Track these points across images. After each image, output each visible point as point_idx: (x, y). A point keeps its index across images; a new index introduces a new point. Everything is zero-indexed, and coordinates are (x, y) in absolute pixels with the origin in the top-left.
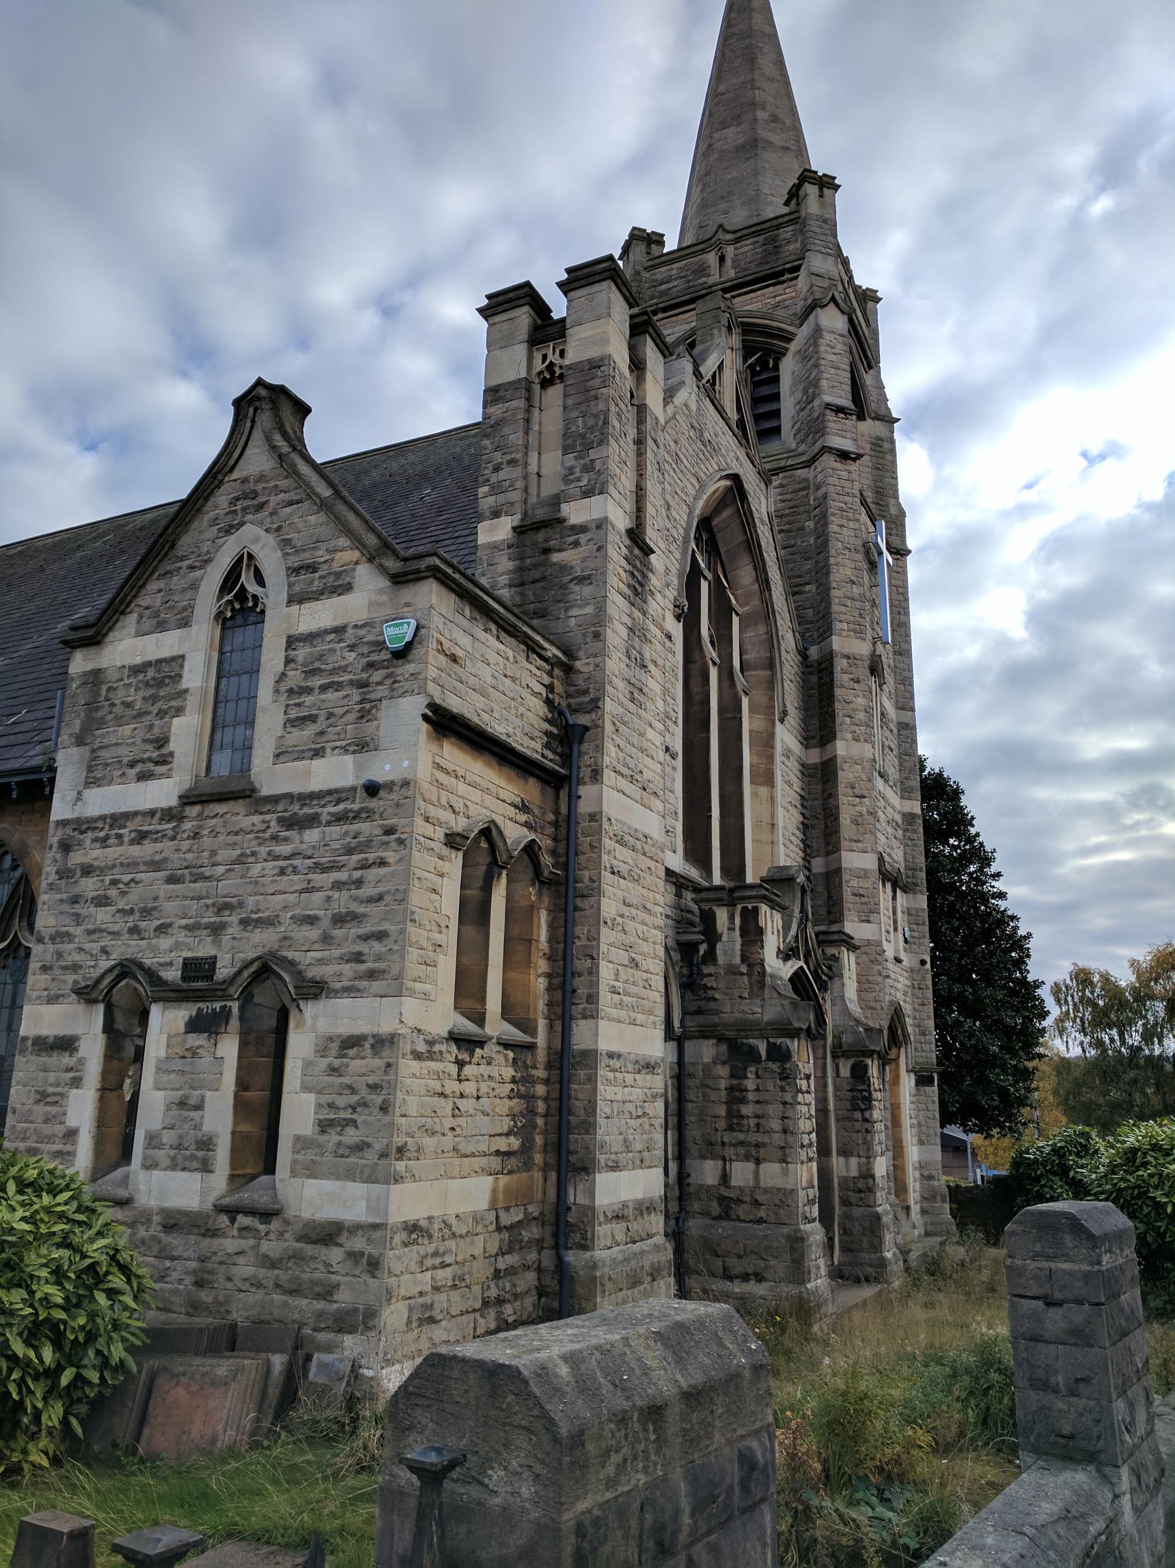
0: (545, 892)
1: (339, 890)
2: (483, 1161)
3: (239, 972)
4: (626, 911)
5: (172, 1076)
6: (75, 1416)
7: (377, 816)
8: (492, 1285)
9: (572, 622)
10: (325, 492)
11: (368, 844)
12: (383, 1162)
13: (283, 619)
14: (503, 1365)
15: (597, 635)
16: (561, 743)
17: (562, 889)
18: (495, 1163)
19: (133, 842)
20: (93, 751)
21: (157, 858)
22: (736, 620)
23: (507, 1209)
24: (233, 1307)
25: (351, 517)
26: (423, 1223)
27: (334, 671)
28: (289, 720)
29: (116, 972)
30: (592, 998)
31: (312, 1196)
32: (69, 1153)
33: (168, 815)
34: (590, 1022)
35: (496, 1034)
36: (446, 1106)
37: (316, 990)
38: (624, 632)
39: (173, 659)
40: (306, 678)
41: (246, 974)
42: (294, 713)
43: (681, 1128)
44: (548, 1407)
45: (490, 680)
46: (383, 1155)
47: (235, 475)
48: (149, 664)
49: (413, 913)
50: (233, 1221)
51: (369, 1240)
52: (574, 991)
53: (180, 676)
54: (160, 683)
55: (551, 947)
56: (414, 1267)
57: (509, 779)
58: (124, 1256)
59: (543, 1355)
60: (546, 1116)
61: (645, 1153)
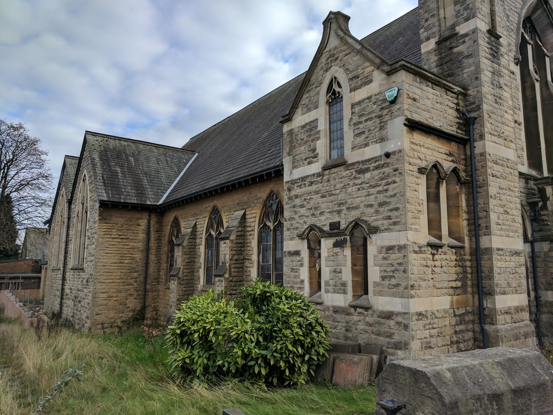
0: (463, 187)
1: (380, 194)
2: (446, 291)
3: (348, 226)
4: (501, 191)
5: (331, 262)
6: (312, 369)
7: (390, 165)
8: (454, 336)
9: (465, 75)
10: (358, 47)
11: (388, 176)
12: (406, 290)
13: (349, 98)
14: (419, 371)
15: (477, 78)
16: (465, 126)
17: (471, 185)
18: (451, 291)
19: (309, 186)
20: (293, 157)
21: (317, 190)
22: (547, 60)
23: (458, 308)
24: (359, 339)
25: (369, 54)
26: (424, 313)
27: (369, 113)
28: (355, 135)
29: (309, 229)
30: (488, 227)
31: (382, 302)
32: (302, 288)
33: (319, 175)
34: (488, 237)
35: (447, 243)
36: (429, 270)
37: (375, 230)
38: (490, 75)
39: (314, 120)
40: (359, 118)
41: (350, 226)
42: (357, 132)
43: (535, 278)
44: (439, 390)
45: (431, 106)
46: (406, 288)
47: (327, 49)
48: (307, 124)
49: (408, 199)
50: (356, 310)
51: (403, 318)
52: (480, 225)
53: (317, 126)
54: (311, 130)
55: (468, 209)
56: (421, 328)
57: (443, 144)
58: (320, 321)
59: (438, 368)
60: (471, 273)
61: (518, 288)
